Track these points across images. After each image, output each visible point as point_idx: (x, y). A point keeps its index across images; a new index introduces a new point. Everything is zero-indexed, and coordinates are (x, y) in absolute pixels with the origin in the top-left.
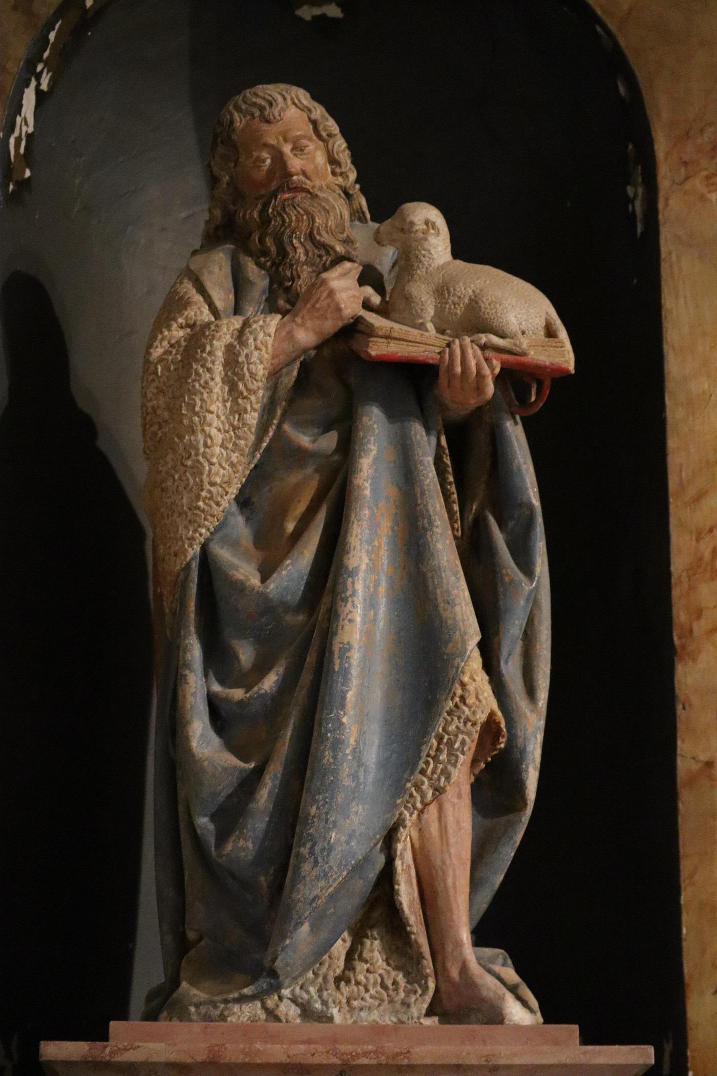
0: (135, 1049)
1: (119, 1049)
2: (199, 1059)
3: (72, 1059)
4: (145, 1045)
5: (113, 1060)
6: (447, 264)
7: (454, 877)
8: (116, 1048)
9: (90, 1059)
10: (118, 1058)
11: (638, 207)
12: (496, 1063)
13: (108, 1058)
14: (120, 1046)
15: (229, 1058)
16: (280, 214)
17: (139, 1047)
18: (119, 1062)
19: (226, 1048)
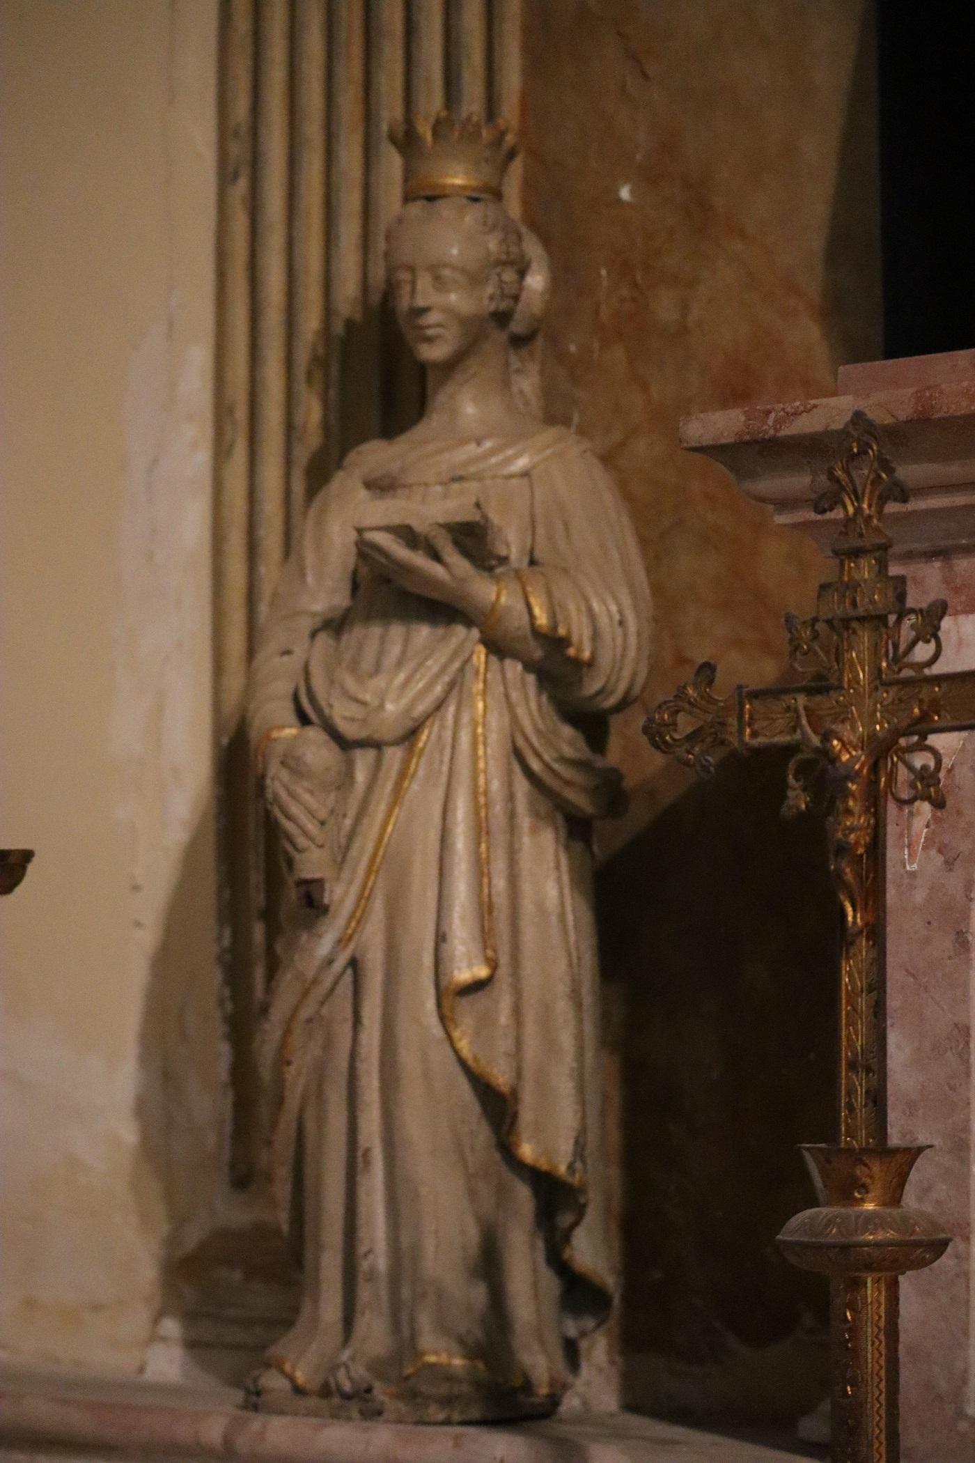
0: (809, 411)
1: (787, 413)
2: (903, 415)
3: (723, 441)
4: (824, 401)
5: (779, 434)
6: (612, 1415)
7: (375, 883)
8: (782, 413)
9: (747, 438)
10: (787, 431)
11: (383, 560)
12: (829, 630)
13: (772, 432)
14: (789, 409)
15: (945, 409)
16: (873, 1427)
17: (815, 406)
18: (792, 437)
19: (941, 392)
